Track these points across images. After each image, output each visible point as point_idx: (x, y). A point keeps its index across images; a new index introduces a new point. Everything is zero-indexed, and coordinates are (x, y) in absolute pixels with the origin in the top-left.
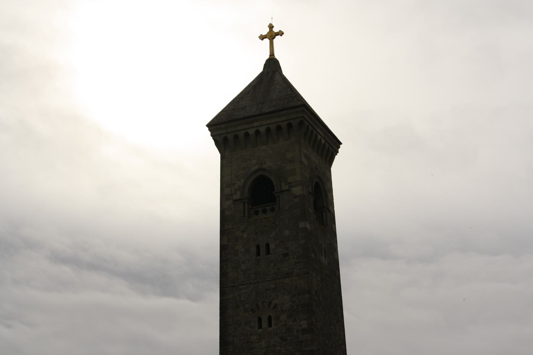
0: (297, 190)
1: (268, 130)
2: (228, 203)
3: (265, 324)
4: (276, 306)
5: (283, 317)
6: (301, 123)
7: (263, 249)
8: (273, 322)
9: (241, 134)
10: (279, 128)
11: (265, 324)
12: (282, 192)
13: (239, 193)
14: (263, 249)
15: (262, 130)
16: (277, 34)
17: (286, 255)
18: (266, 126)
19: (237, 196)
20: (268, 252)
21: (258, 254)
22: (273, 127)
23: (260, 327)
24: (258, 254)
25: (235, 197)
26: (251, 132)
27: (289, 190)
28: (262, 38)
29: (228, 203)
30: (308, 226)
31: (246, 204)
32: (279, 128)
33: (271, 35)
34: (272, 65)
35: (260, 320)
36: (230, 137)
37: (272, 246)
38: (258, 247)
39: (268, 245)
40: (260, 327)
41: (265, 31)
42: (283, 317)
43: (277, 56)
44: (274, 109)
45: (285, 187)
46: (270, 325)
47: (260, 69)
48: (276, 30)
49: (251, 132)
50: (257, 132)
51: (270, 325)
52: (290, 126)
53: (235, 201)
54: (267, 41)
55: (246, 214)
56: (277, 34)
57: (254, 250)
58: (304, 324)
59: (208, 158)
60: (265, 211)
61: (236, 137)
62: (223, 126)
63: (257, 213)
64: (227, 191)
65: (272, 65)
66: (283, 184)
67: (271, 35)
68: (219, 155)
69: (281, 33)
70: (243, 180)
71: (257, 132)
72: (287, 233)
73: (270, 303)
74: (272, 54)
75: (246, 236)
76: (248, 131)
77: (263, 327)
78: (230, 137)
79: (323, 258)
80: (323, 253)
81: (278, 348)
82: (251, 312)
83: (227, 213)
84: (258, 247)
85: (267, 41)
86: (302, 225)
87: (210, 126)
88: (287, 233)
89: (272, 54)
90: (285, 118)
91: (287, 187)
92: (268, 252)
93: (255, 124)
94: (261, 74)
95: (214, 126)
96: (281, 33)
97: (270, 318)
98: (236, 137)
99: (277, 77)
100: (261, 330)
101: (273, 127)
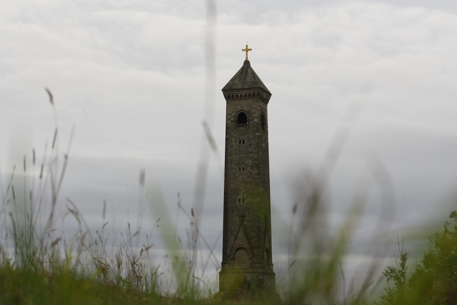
0: (256, 120)
1: (246, 95)
2: (229, 122)
3: (242, 170)
4: (246, 164)
5: (249, 168)
6: (258, 94)
7: (242, 141)
9: (235, 95)
10: (250, 95)
11: (242, 170)
12: (250, 120)
13: (233, 118)
14: (242, 141)
15: (243, 95)
16: (249, 50)
17: (250, 145)
19: (233, 119)
20: (244, 143)
21: (240, 143)
22: (248, 94)
23: (240, 171)
24: (240, 143)
26: (239, 95)
27: (252, 120)
28: (243, 50)
29: (229, 122)
30: (259, 134)
32: (250, 95)
33: (247, 50)
34: (247, 63)
35: (240, 168)
36: (231, 96)
37: (245, 141)
38: (240, 140)
39: (244, 140)
40: (240, 171)
41: (245, 48)
42: (249, 168)
43: (249, 60)
44: (248, 87)
46: (244, 171)
47: (242, 65)
49: (239, 95)
50: (241, 95)
51: (244, 171)
52: (254, 94)
53: (232, 121)
54: (245, 52)
56: (249, 50)
57: (238, 141)
58: (256, 172)
59: (221, 103)
60: (243, 126)
61: (233, 96)
63: (240, 126)
64: (229, 117)
65: (247, 63)
67: (247, 50)
68: (226, 102)
69: (251, 50)
70: (235, 113)
71: (241, 95)
72: (251, 136)
73: (244, 162)
74: (247, 58)
78: (231, 96)
79: (131, 275)
80: (98, 266)
83: (229, 126)
84: (240, 140)
85: (245, 52)
86: (257, 134)
88: (251, 136)
89: (247, 58)
90: (252, 91)
91: (252, 119)
92: (244, 143)
93: (241, 92)
94: (243, 67)
95: (223, 90)
96: (251, 50)
97: (244, 168)
98: (233, 96)
99: (249, 71)
101: (248, 94)
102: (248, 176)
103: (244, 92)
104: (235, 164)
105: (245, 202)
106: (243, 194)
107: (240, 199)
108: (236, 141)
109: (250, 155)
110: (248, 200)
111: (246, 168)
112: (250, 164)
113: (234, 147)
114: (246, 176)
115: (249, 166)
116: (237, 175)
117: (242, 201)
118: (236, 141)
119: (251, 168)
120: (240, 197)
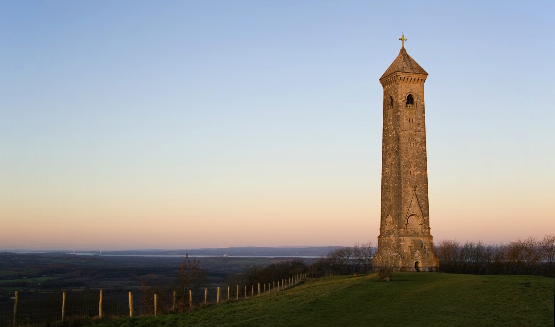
3: (412, 146)
5: (418, 144)
7: (411, 120)
11: (412, 146)
19: (404, 99)
42: (418, 144)
108: (407, 119)
112: (419, 141)
116: (409, 149)
118: (407, 119)
120: (412, 169)
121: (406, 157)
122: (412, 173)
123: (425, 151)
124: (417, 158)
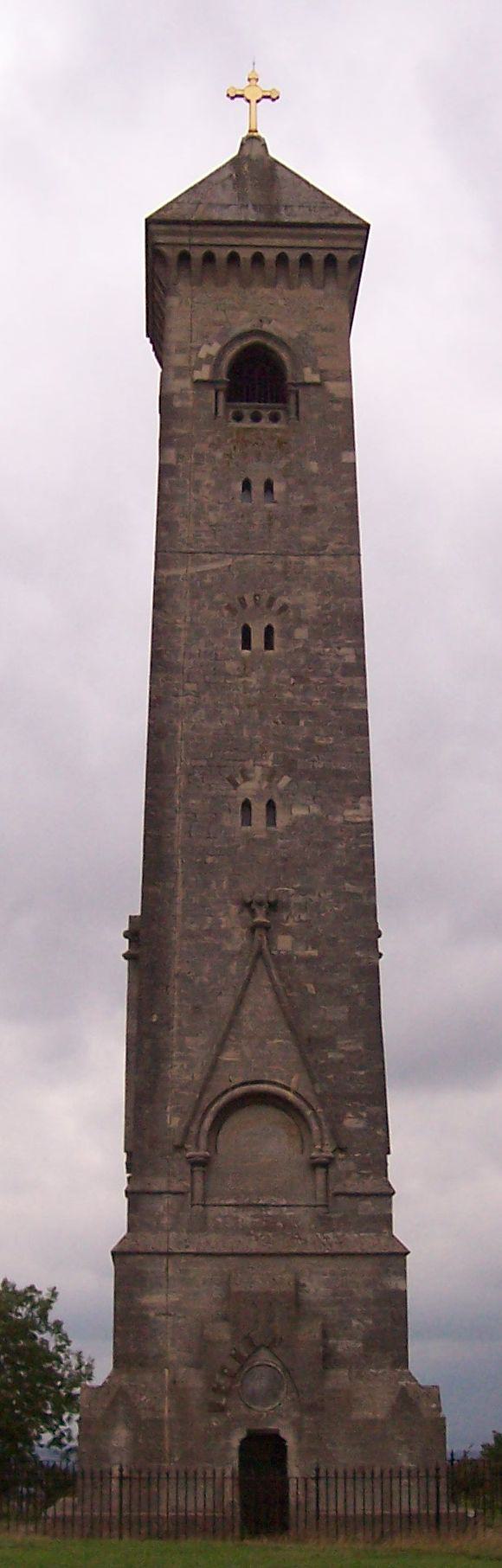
3: (257, 640)
4: (284, 608)
5: (301, 633)
8: (277, 639)
10: (306, 260)
18: (279, 251)
19: (204, 373)
25: (198, 375)
26: (246, 255)
31: (221, 396)
35: (246, 632)
37: (278, 487)
45: (310, 376)
46: (269, 645)
48: (241, 85)
51: (269, 645)
55: (221, 413)
60: (256, 418)
62: (185, 228)
63: (256, 418)
66: (308, 370)
72: (314, 467)
73: (271, 601)
75: (219, 455)
76: (215, 250)
77: (253, 645)
81: (289, 695)
82: (226, 612)
87: (368, 226)
91: (316, 378)
93: (257, 241)
97: (269, 631)
100: (246, 652)
102: (299, 678)
103: (277, 242)
104: (215, 606)
105: (282, 819)
106: (271, 775)
107: (247, 805)
109: (312, 561)
110: (299, 812)
111: (289, 635)
112: (309, 612)
113: (212, 518)
114: (284, 674)
115: (300, 622)
117: (259, 809)
119: (315, 634)
121: (213, 715)
122: (259, 809)
123: (360, 669)
124: (291, 715)
